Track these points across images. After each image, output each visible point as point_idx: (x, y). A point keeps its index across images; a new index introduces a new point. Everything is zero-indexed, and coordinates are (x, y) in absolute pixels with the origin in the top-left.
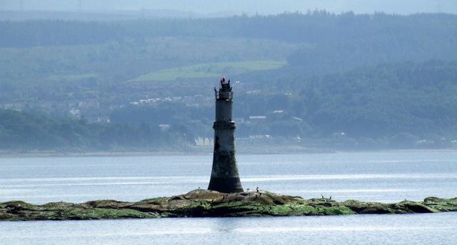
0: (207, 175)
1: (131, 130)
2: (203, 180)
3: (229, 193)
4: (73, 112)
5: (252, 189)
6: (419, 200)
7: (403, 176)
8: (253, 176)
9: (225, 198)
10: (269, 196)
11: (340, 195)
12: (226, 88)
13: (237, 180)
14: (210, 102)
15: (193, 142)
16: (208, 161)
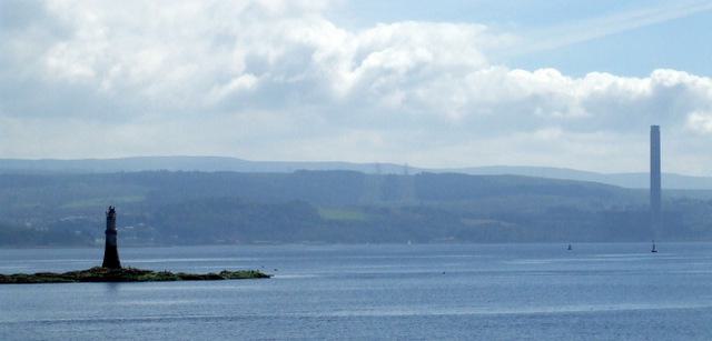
0: (99, 246)
1: (61, 236)
2: (99, 262)
3: (701, 76)
4: (28, 224)
5: (126, 267)
6: (218, 273)
7: (219, 259)
8: (126, 262)
9: (112, 272)
10: (136, 270)
11: (233, 268)
12: (112, 212)
13: (119, 262)
14: (104, 219)
15: (94, 240)
16: (102, 252)
